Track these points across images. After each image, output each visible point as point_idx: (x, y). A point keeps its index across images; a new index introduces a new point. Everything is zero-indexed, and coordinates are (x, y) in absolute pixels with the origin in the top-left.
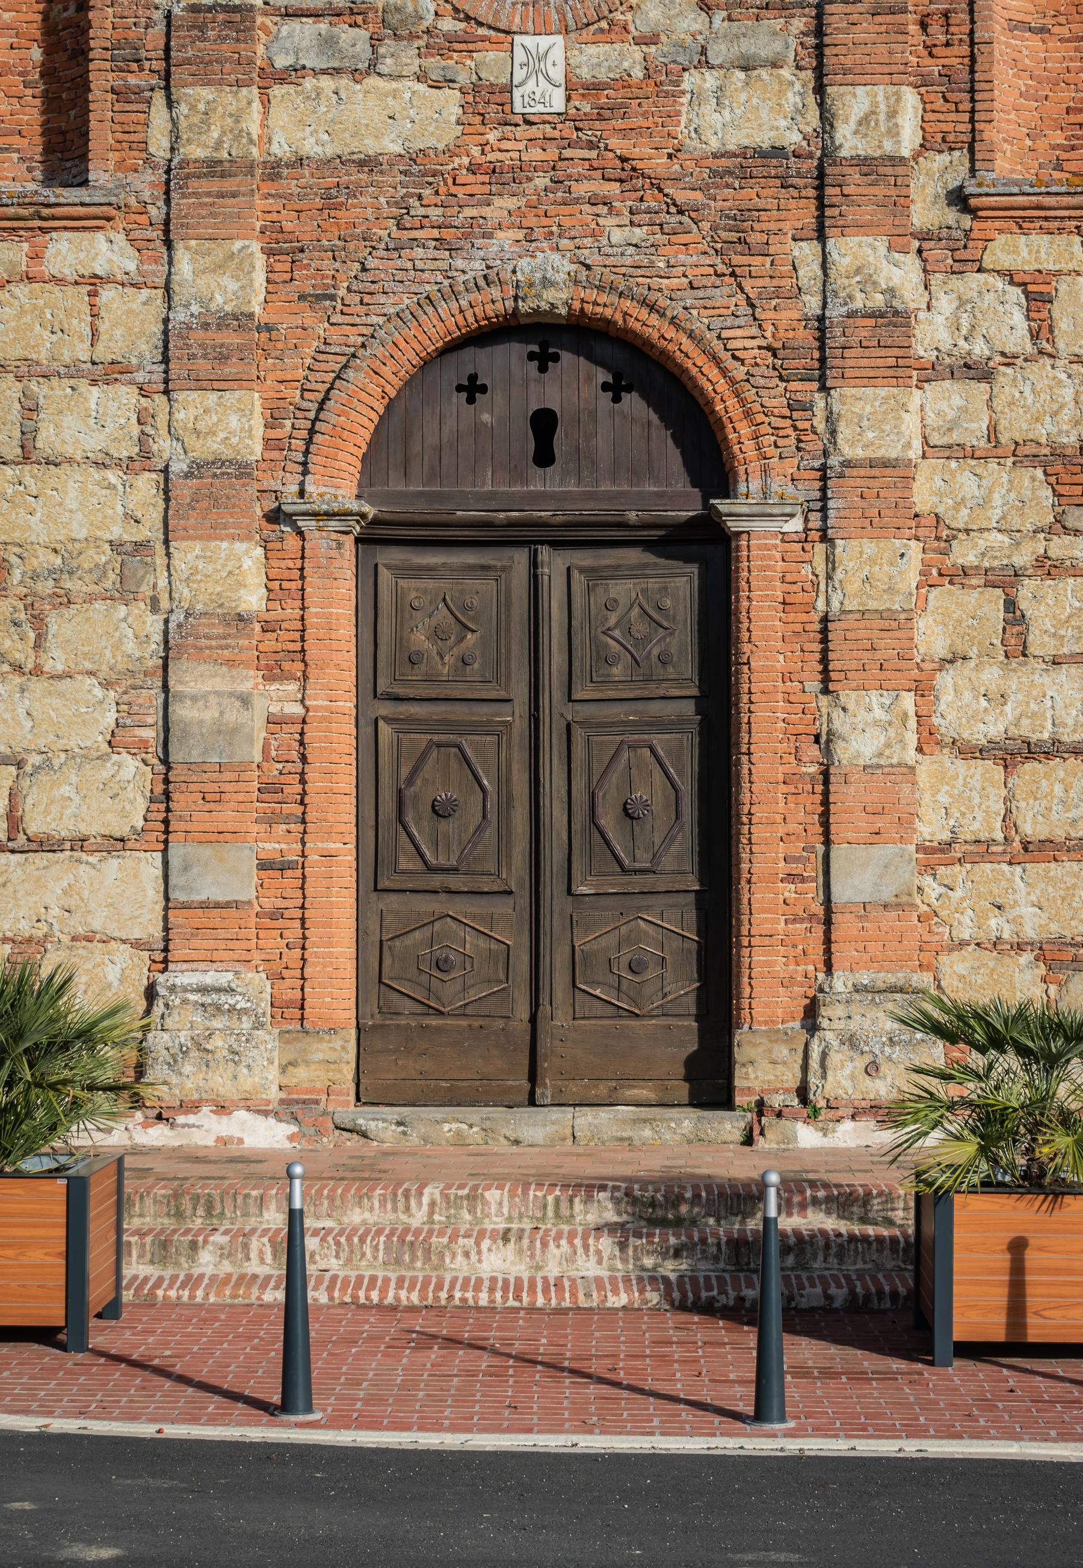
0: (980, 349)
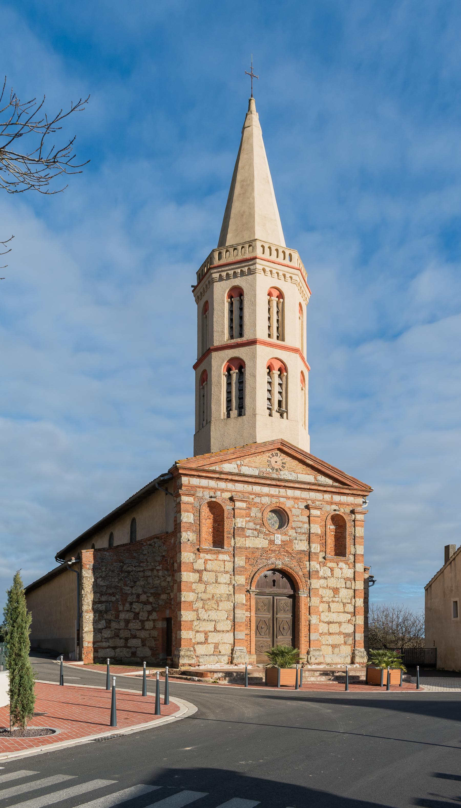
0: (326, 576)
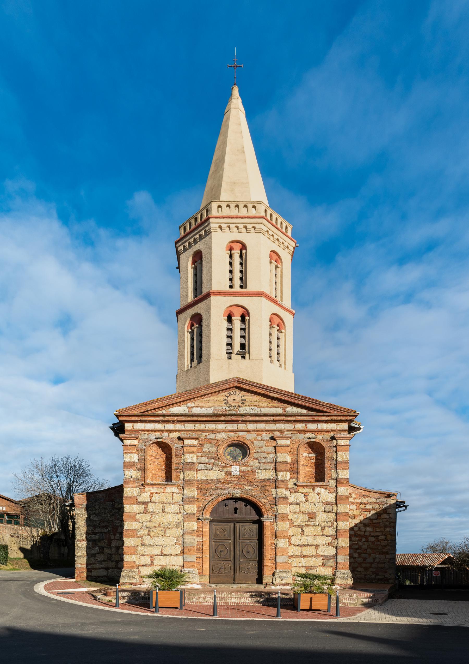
0: (298, 501)
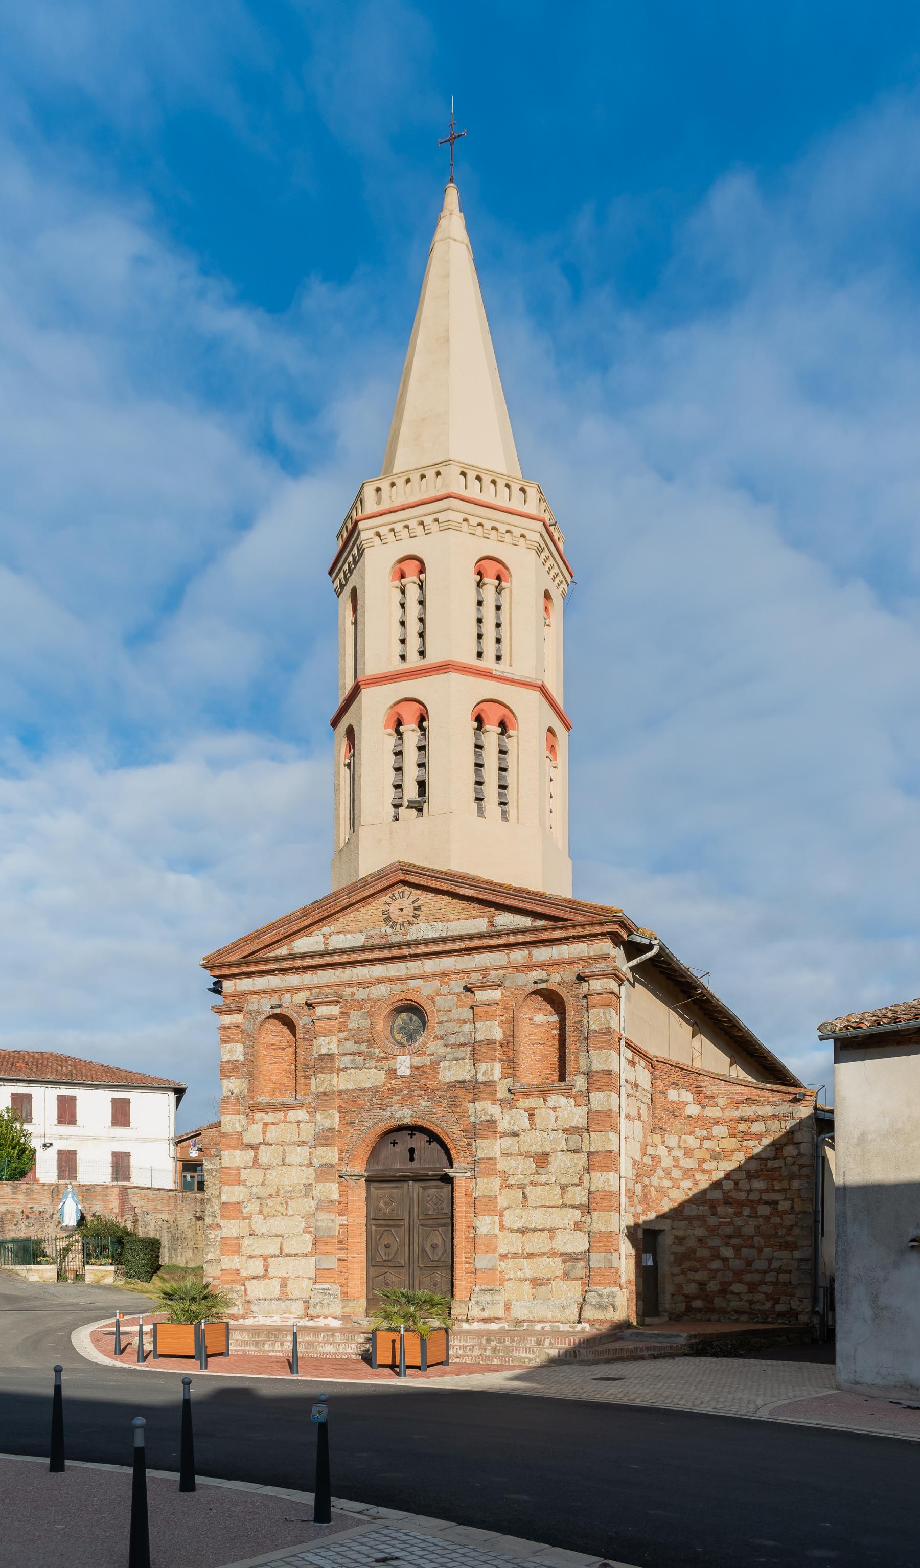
0: (516, 1129)
